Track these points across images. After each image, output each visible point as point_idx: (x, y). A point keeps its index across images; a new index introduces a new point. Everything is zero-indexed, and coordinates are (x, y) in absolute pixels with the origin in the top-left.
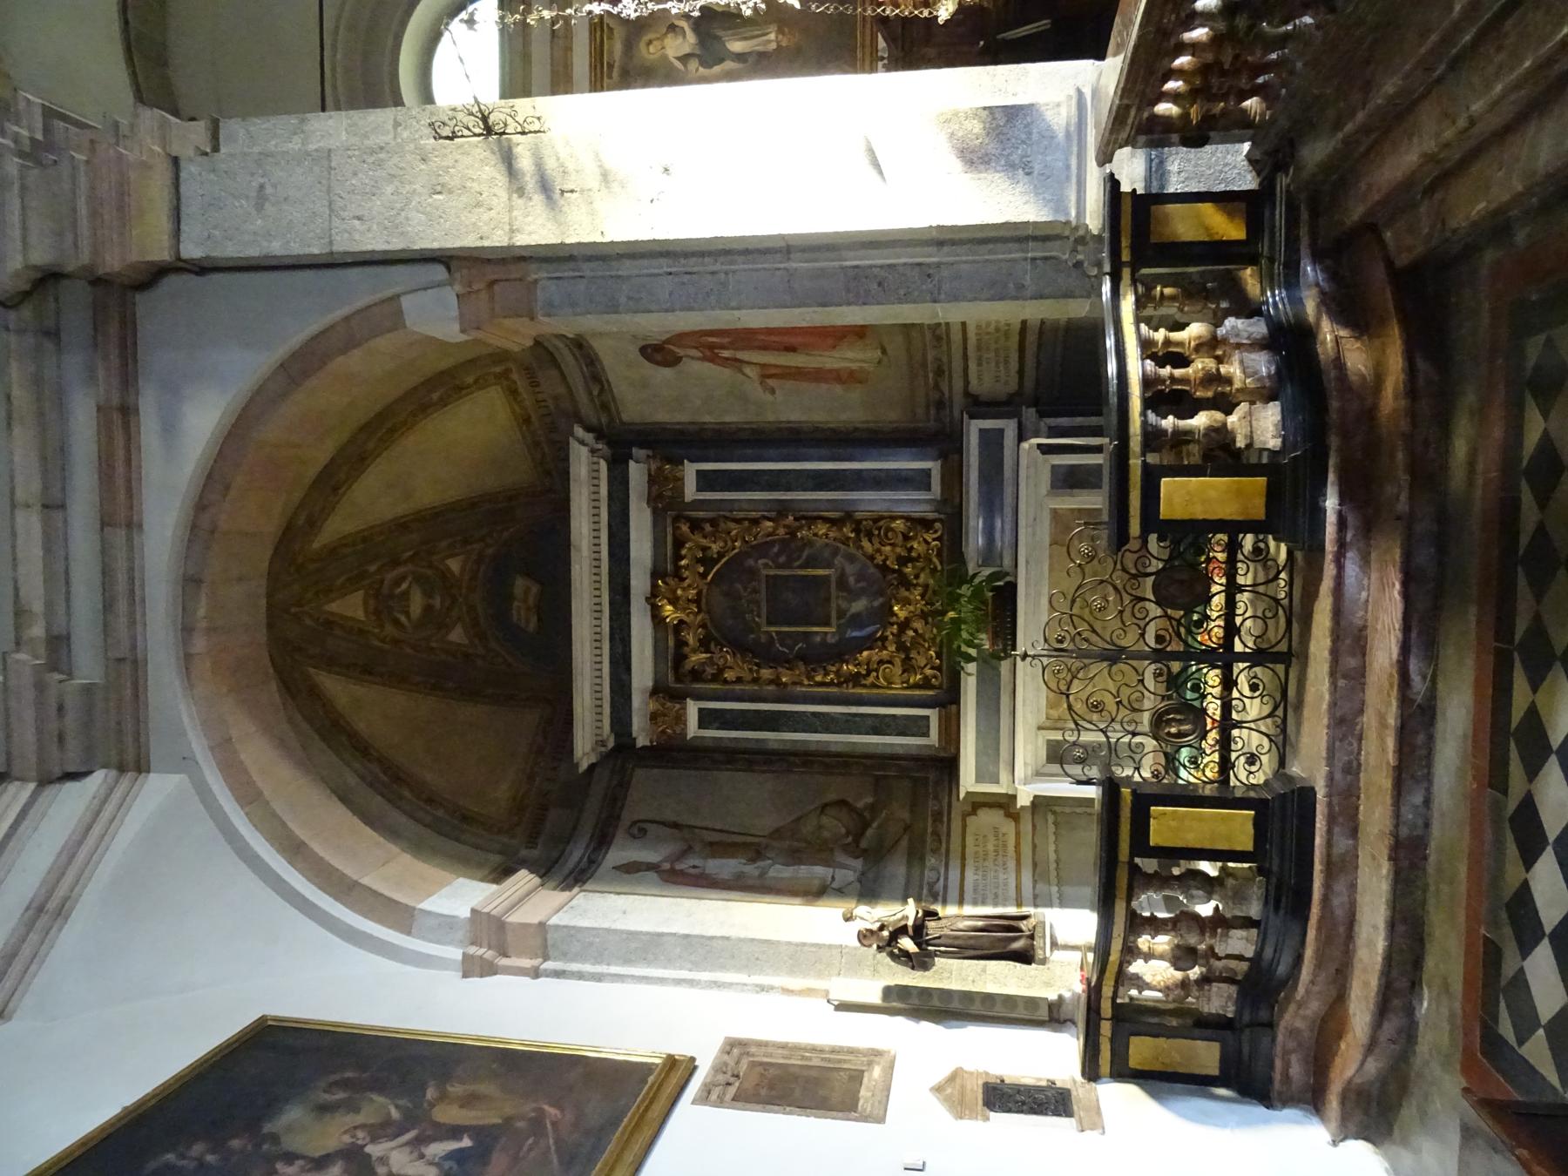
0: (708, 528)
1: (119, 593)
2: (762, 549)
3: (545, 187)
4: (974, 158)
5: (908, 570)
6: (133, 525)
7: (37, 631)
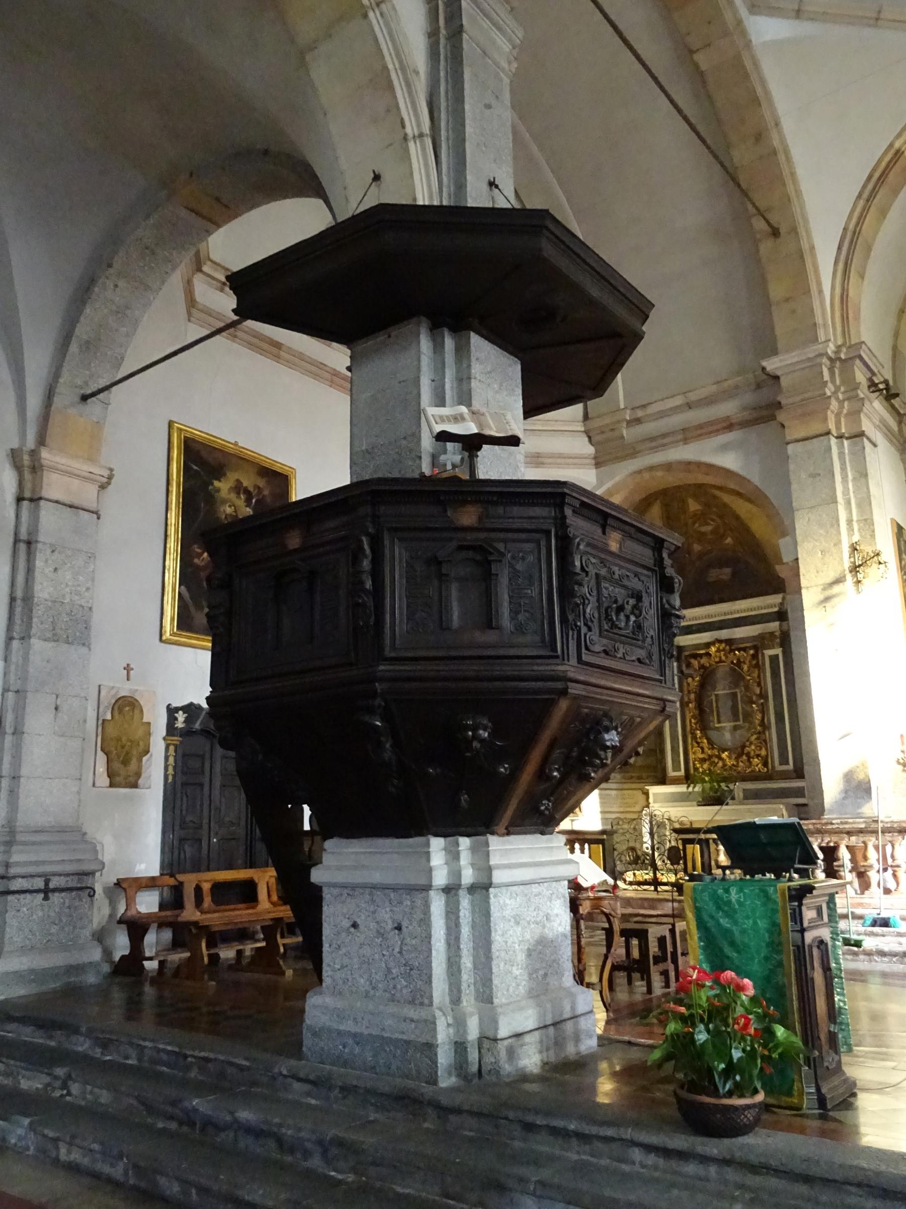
0: (754, 662)
1: (657, 441)
2: (747, 688)
3: (827, 599)
4: (848, 777)
5: (745, 757)
6: (686, 441)
7: (640, 413)
